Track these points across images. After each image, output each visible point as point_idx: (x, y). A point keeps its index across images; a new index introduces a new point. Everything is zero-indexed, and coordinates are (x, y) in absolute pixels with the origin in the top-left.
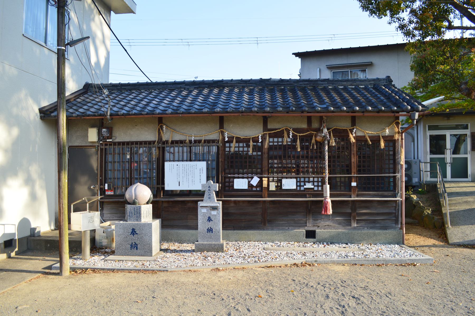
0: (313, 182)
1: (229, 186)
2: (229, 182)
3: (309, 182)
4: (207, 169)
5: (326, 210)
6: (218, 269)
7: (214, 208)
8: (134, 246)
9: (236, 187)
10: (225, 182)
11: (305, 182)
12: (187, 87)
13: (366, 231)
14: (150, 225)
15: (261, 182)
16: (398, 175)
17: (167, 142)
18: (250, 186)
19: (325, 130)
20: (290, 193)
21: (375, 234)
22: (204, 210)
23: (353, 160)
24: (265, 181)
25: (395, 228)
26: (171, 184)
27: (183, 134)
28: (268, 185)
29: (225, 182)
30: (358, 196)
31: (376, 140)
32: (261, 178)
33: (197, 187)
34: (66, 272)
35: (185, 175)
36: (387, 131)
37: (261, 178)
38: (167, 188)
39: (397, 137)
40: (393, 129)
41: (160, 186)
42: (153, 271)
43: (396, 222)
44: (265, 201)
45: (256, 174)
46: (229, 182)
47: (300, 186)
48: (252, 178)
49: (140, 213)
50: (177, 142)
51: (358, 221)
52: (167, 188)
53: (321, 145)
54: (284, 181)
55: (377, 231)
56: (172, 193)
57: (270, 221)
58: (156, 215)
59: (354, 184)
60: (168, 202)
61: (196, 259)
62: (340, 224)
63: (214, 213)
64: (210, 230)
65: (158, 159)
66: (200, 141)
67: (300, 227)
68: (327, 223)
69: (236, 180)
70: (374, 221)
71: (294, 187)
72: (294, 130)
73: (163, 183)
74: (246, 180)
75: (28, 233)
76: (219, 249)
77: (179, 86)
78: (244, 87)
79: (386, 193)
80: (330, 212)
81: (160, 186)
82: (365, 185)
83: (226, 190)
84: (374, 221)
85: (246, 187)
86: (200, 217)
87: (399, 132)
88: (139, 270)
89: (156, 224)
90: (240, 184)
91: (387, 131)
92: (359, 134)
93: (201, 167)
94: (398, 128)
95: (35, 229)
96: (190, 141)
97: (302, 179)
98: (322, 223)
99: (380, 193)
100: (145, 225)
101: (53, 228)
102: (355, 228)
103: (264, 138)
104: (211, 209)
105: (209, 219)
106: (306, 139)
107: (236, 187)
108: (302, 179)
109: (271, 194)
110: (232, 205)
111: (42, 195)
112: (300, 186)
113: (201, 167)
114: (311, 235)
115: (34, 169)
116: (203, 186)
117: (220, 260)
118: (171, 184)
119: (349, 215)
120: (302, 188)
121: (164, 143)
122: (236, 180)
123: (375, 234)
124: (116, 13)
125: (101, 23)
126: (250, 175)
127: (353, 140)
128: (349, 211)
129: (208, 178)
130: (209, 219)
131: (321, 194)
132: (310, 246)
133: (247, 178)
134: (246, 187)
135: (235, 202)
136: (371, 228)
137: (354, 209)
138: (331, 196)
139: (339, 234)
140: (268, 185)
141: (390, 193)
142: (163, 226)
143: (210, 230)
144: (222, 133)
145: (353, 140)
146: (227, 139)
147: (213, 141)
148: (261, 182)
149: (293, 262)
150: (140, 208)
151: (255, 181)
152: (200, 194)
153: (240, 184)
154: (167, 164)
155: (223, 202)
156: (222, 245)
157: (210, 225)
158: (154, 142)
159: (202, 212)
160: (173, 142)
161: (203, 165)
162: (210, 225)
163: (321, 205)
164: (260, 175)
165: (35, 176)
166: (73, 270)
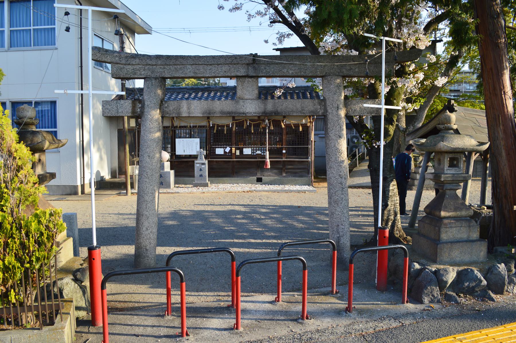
0: (261, 150)
1: (213, 153)
2: (213, 150)
3: (259, 150)
4: (200, 143)
5: (266, 166)
6: (204, 193)
7: (203, 164)
8: (162, 183)
9: (217, 153)
10: (211, 150)
11: (256, 150)
12: (188, 91)
13: (290, 178)
14: (169, 172)
15: (231, 150)
16: (310, 146)
17: (177, 127)
18: (225, 152)
19: (267, 121)
20: (247, 156)
21: (295, 180)
22: (198, 165)
23: (284, 138)
24: (234, 149)
25: (307, 177)
26: (179, 151)
27: (186, 122)
28: (235, 152)
29: (211, 150)
30: (286, 158)
31: (297, 126)
32: (231, 148)
33: (194, 153)
34: (129, 194)
35: (188, 146)
36: (304, 121)
37: (231, 148)
38: (177, 153)
39: (309, 124)
40: (307, 120)
41: (173, 153)
42: (172, 193)
43: (308, 173)
44: (233, 161)
45: (229, 145)
46: (213, 150)
47: (254, 152)
48: (226, 148)
49: (164, 167)
50: (182, 127)
51: (286, 173)
52: (177, 153)
53: (264, 129)
54: (244, 150)
55: (297, 178)
56: (180, 157)
57: (237, 173)
58: (171, 169)
59: (284, 151)
60: (178, 162)
61: (195, 189)
62: (276, 174)
63: (203, 166)
64: (201, 176)
65: (172, 137)
66: (196, 127)
67: (253, 176)
68: (269, 174)
69: (217, 149)
70: (295, 173)
71: (250, 153)
72: (250, 120)
73: (175, 151)
74: (223, 149)
75: (100, 179)
76: (206, 185)
77: (183, 90)
78: (224, 91)
79: (302, 157)
80: (269, 166)
81: (173, 153)
82: (292, 152)
83: (210, 155)
84: (295, 173)
85: (223, 153)
86: (195, 169)
87: (310, 122)
88: (165, 193)
89: (172, 172)
90: (219, 151)
91: (304, 121)
92: (288, 123)
93: (196, 141)
94: (310, 119)
95: (103, 177)
96: (190, 127)
97: (255, 149)
98: (266, 174)
99: (299, 157)
100: (167, 172)
101: (110, 177)
102: (284, 177)
103: (232, 125)
104: (202, 165)
105: (201, 170)
106: (257, 126)
107: (217, 153)
108: (255, 149)
109: (237, 157)
110: (215, 163)
111: (105, 157)
112: (254, 152)
113: (196, 141)
114: (259, 180)
115: (101, 142)
116: (197, 152)
117: (205, 189)
118: (179, 151)
119: (281, 169)
120: (255, 154)
121: (175, 127)
122: (217, 149)
123: (295, 180)
124: (138, 34)
125: (209, 244)
126: (225, 146)
127: (283, 126)
128: (281, 167)
129: (201, 148)
130: (201, 170)
131: (264, 157)
132: (260, 187)
133: (223, 148)
134: (223, 153)
135: (216, 161)
136: (294, 176)
137: (284, 166)
138: (270, 158)
139: (275, 179)
140: (235, 152)
141: (305, 157)
142: (176, 176)
143: (201, 176)
144: (209, 122)
145: (283, 126)
146: (211, 125)
147: (204, 126)
148: (231, 150)
149: (243, 190)
150: (164, 163)
151: (228, 150)
152: (195, 157)
153: (219, 151)
154: (177, 140)
155: (208, 161)
156: (208, 183)
157: (201, 173)
158: (169, 127)
159: (197, 166)
160: (180, 127)
161: (198, 140)
162: (201, 173)
163: (264, 163)
164: (231, 146)
165: (101, 146)
166: (132, 193)
